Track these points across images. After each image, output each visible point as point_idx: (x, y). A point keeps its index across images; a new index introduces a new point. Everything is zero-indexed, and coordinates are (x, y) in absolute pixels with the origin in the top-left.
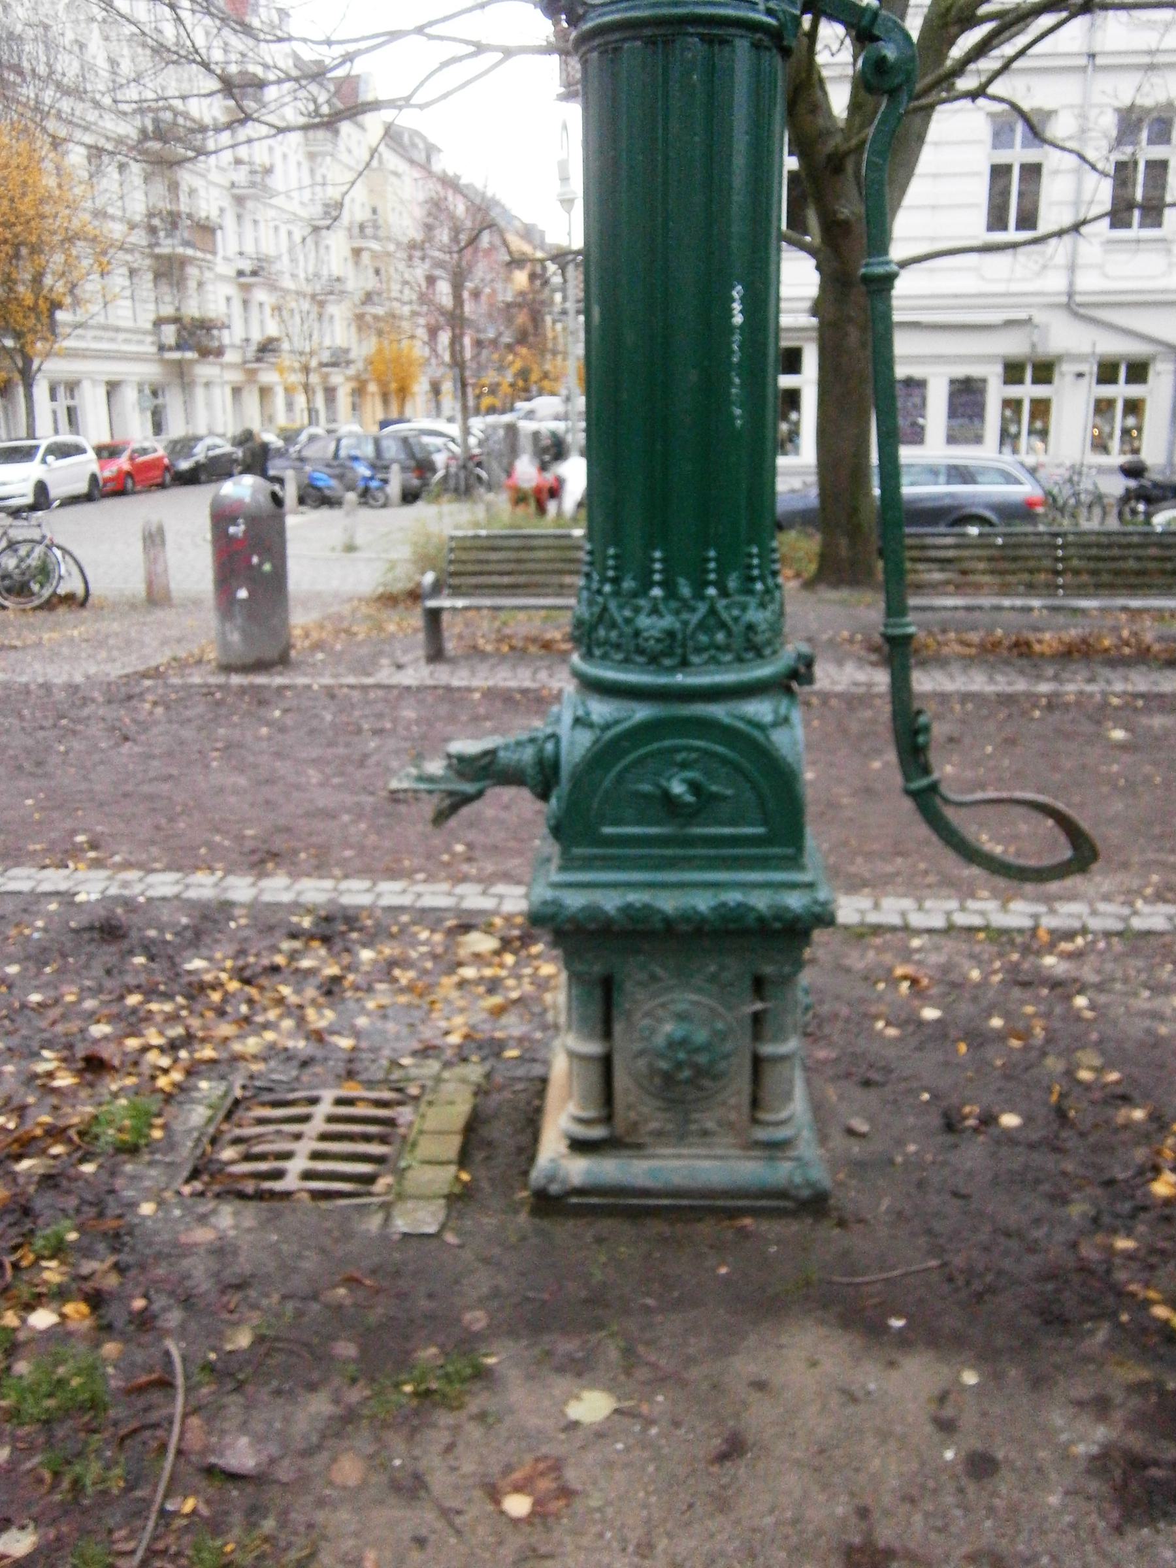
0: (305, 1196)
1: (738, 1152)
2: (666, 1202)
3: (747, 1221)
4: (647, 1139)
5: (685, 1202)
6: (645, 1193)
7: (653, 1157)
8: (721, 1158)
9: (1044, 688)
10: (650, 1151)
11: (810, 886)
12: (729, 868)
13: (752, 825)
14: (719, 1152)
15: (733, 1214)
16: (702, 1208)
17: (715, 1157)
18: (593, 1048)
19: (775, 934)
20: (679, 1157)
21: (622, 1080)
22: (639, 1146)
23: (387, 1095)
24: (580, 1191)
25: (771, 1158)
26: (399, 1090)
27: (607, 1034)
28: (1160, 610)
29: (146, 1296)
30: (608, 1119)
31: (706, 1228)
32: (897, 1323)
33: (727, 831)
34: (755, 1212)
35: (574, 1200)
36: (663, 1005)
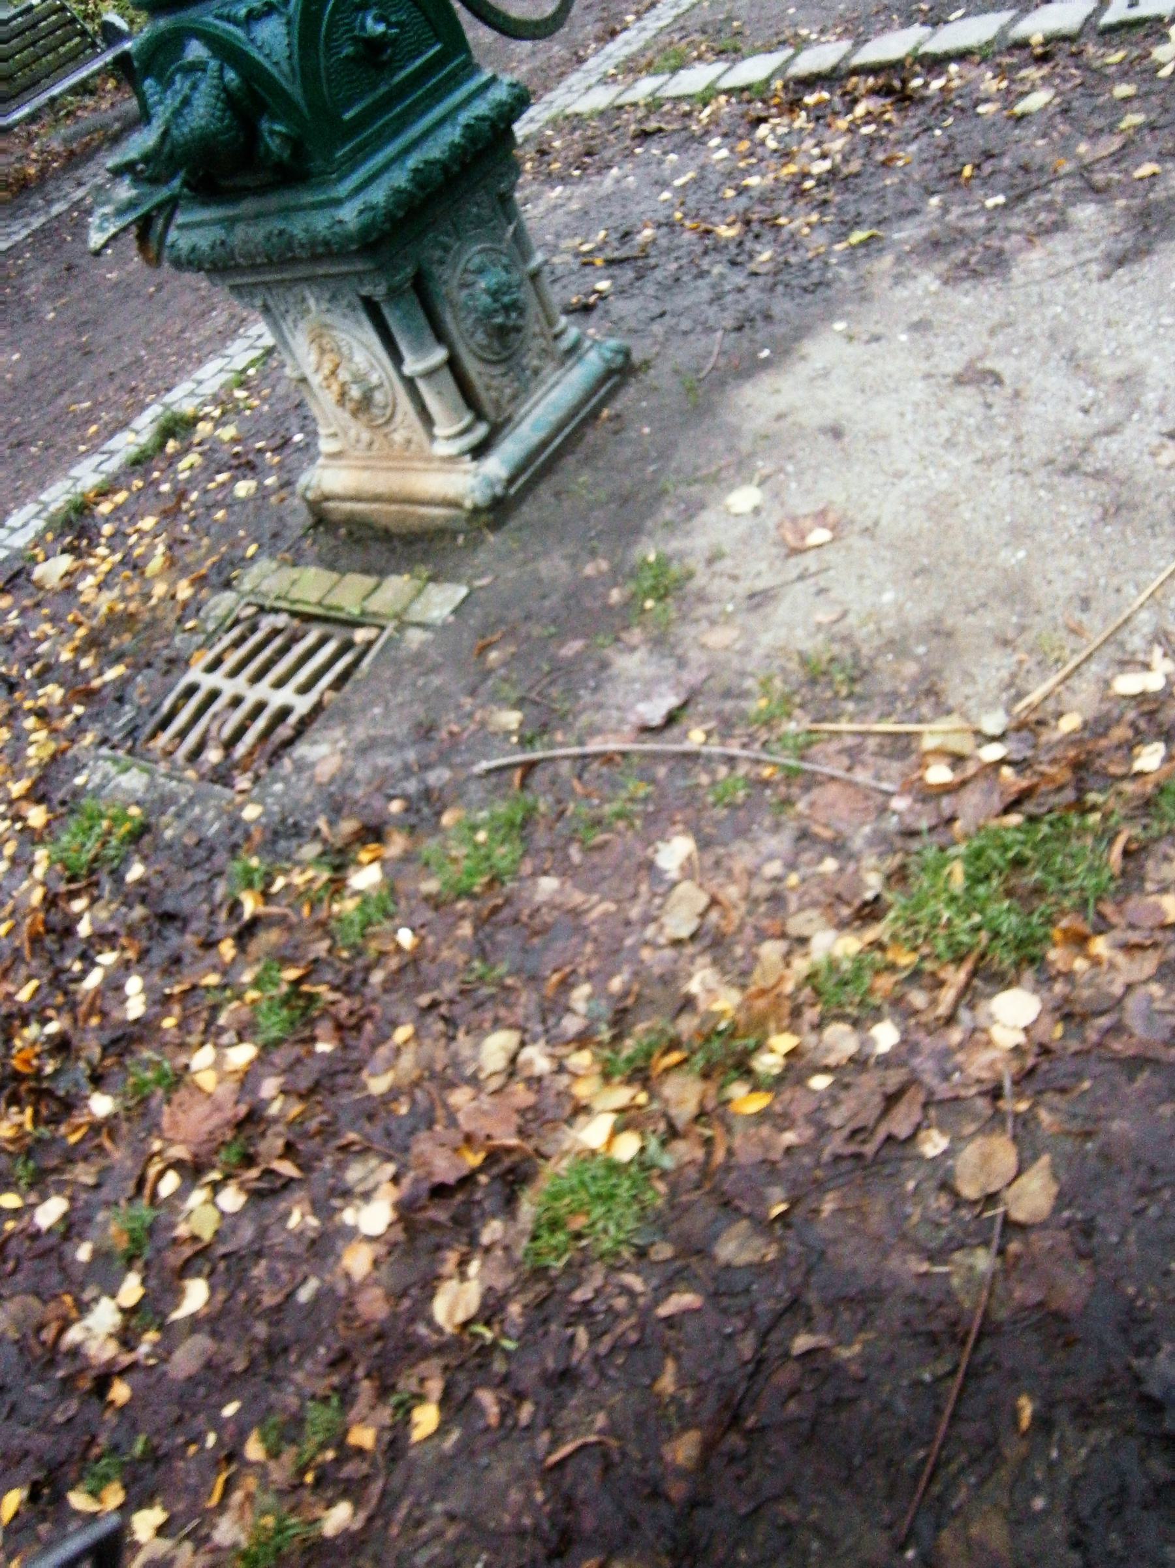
0: (330, 695)
1: (558, 373)
2: (558, 441)
3: (605, 413)
4: (509, 410)
5: (567, 430)
6: (544, 444)
7: (523, 418)
8: (557, 383)
9: (58, 208)
10: (517, 418)
11: (493, 80)
12: (439, 101)
13: (432, 46)
14: (551, 381)
15: (594, 415)
16: (575, 431)
17: (553, 386)
18: (439, 355)
19: (479, 156)
20: (536, 404)
21: (472, 367)
22: (509, 419)
23: (236, 633)
24: (511, 481)
25: (580, 358)
26: (237, 622)
27: (441, 337)
28: (83, 83)
29: (391, 798)
30: (480, 416)
31: (592, 436)
32: (765, 353)
33: (419, 62)
34: (603, 403)
35: (512, 491)
36: (465, 271)
